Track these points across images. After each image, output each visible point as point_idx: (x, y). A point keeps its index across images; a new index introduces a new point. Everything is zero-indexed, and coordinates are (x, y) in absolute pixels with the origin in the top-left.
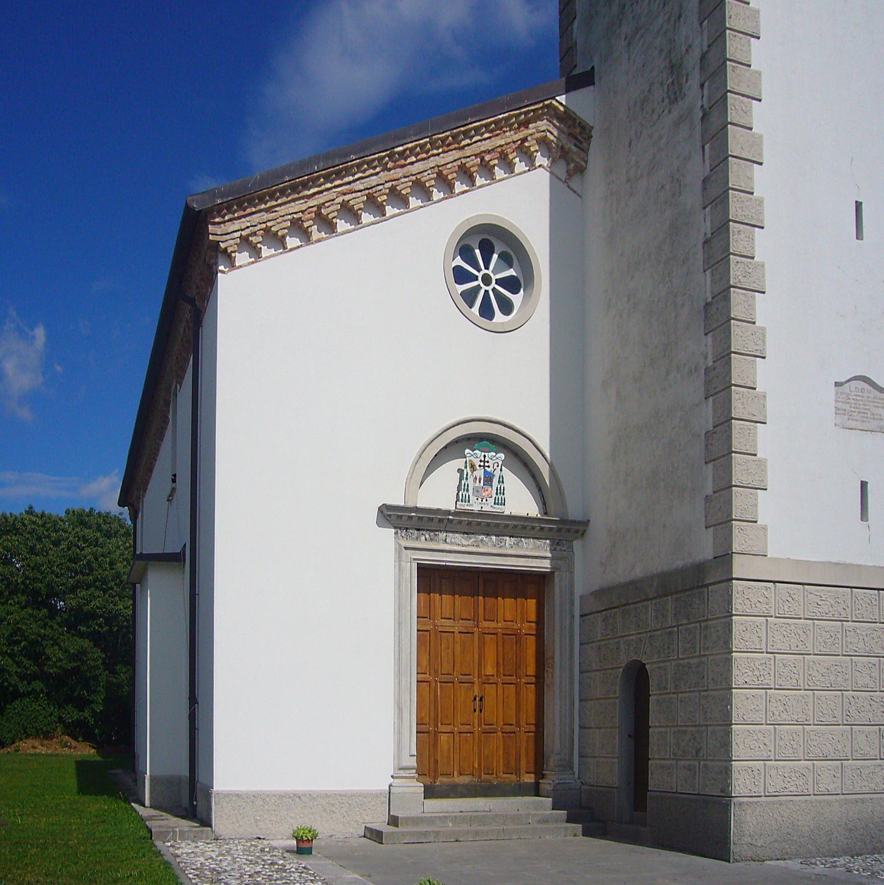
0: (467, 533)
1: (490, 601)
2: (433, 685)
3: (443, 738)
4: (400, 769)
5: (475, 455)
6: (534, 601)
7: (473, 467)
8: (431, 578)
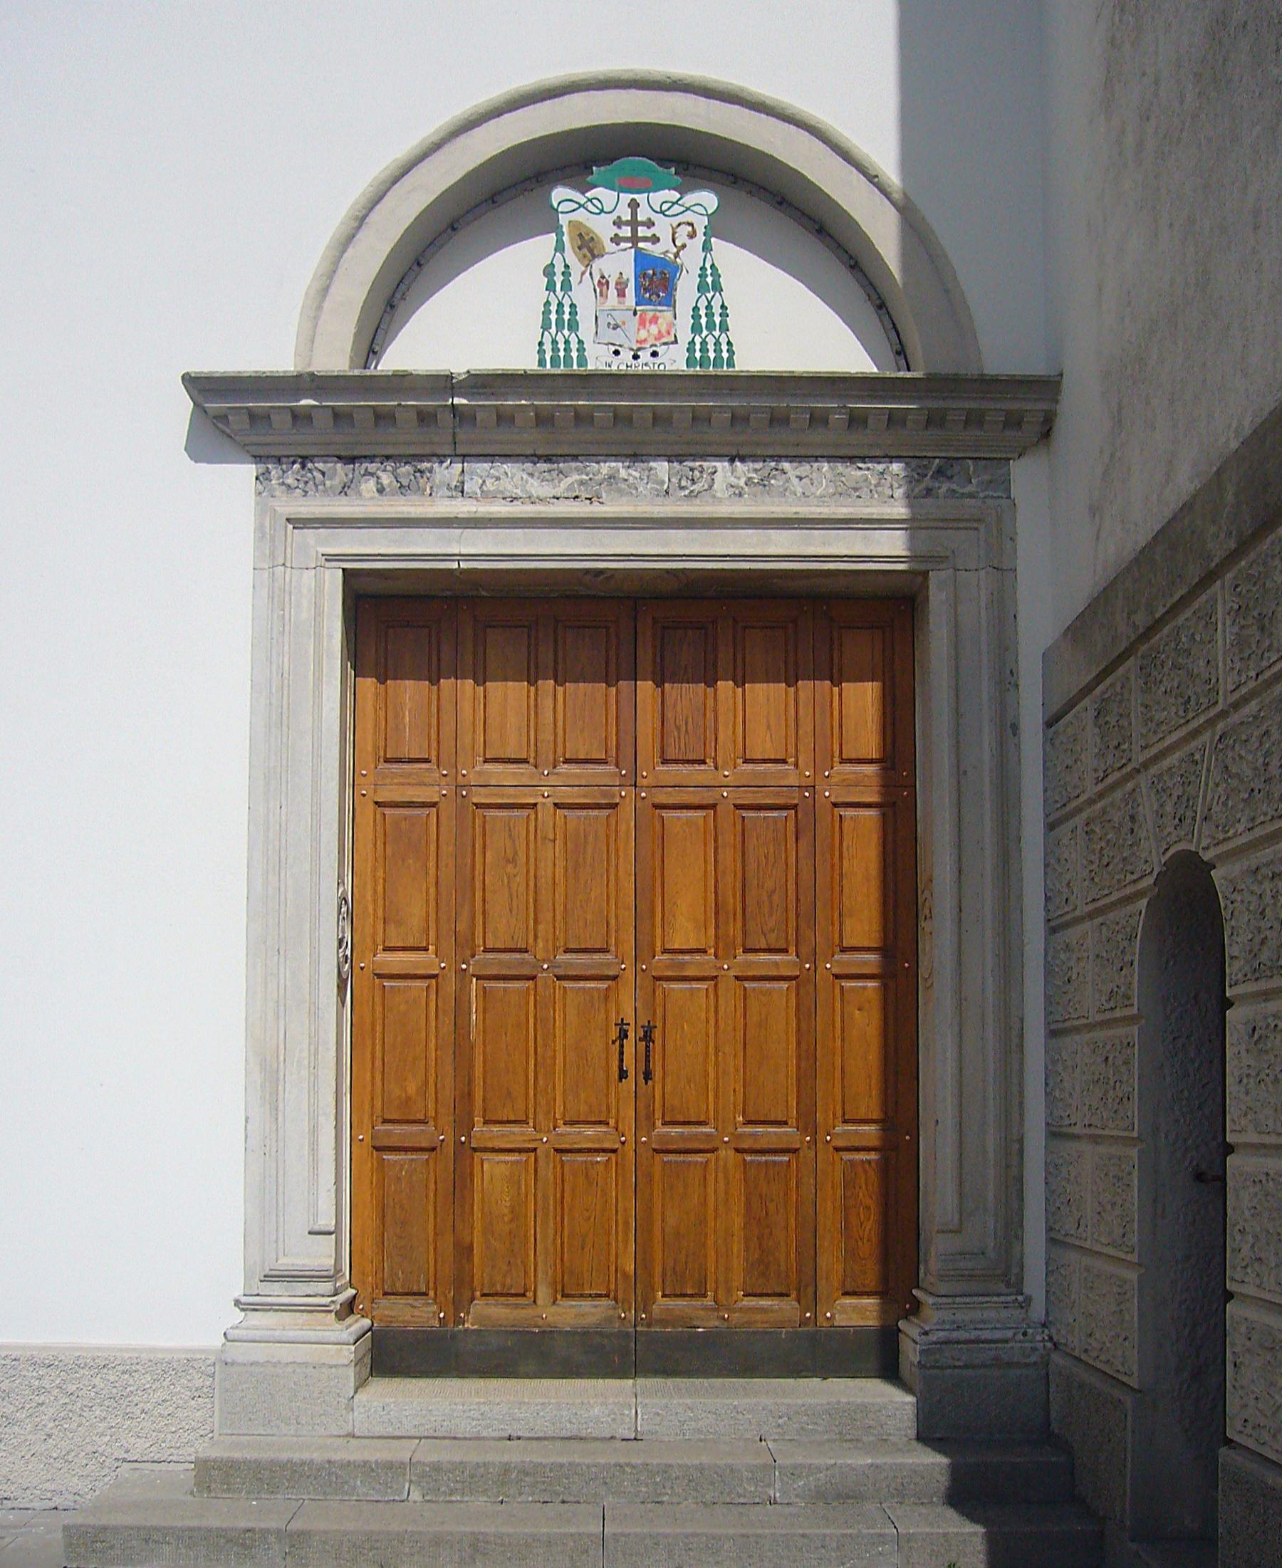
0: (548, 459)
1: (686, 695)
2: (451, 987)
3: (492, 1170)
4: (267, 1278)
5: (596, 207)
6: (877, 685)
7: (588, 247)
8: (396, 622)
